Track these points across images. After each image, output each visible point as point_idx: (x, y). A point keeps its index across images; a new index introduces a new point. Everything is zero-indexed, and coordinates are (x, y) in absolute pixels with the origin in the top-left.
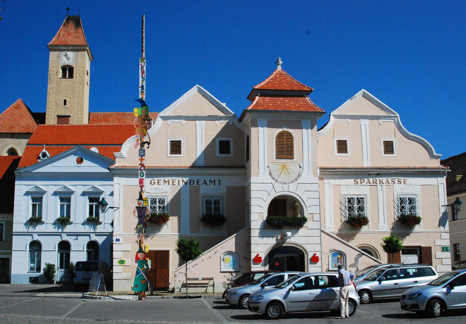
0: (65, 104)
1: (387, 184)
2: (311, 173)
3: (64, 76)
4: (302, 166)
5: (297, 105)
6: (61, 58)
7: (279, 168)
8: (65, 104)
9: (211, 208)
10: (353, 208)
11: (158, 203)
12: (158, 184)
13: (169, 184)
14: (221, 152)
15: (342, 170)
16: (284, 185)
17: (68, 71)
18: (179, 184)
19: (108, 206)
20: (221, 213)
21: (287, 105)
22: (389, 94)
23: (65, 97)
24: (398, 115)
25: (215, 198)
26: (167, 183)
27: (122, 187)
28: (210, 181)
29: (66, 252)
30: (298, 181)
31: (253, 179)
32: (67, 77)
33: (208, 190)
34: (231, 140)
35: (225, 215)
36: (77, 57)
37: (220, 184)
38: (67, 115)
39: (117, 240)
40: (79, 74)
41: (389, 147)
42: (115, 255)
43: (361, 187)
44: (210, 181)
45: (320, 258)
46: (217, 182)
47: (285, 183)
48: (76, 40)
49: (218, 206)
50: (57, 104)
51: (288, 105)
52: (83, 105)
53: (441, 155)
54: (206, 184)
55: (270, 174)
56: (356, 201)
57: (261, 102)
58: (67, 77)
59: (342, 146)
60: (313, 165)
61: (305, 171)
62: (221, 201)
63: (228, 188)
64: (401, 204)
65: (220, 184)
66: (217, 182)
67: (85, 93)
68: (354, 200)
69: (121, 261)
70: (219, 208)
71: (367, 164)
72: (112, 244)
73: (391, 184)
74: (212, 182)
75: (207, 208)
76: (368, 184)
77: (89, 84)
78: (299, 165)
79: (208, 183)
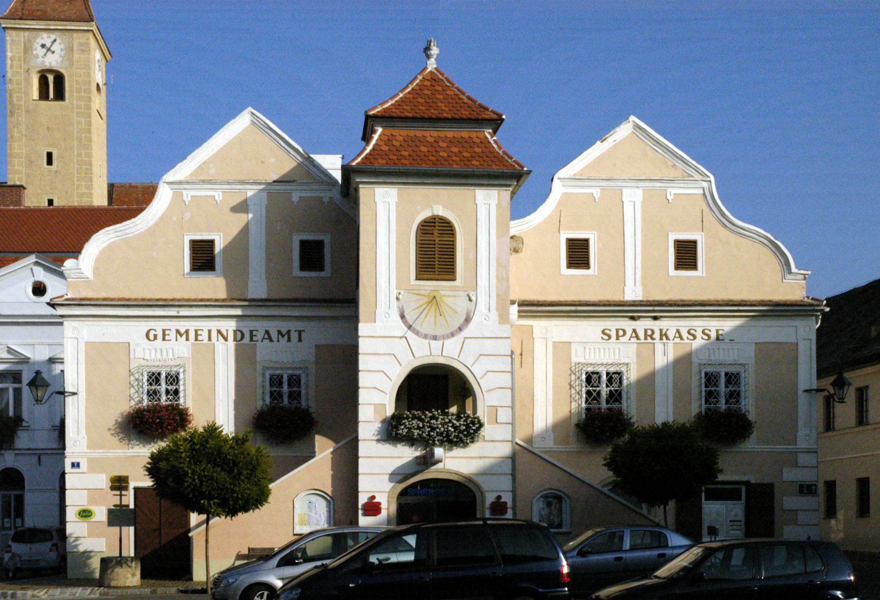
0: (50, 161)
1: (678, 340)
2: (494, 315)
3: (44, 95)
4: (473, 298)
5: (465, 154)
6: (35, 52)
7: (421, 302)
8: (50, 161)
9: (280, 395)
10: (718, 393)
11: (163, 383)
12: (164, 339)
13: (187, 339)
14: (303, 268)
15: (573, 308)
16: (433, 342)
17: (53, 86)
18: (210, 339)
19: (50, 390)
20: (304, 403)
21: (442, 154)
22: (688, 130)
23: (50, 145)
24: (712, 178)
25: (290, 372)
26: (184, 336)
27: (82, 346)
28: (279, 332)
29: (17, 493)
30: (466, 333)
31: (364, 328)
32: (51, 95)
33: (266, 352)
34: (327, 239)
35: (751, 417)
36: (70, 49)
37: (300, 340)
38: (18, 183)
39: (73, 465)
40: (79, 91)
41: (686, 255)
42: (71, 498)
43: (617, 346)
44: (279, 332)
45: (510, 504)
46: (294, 336)
47: (435, 338)
48: (66, 8)
49: (295, 389)
50: (32, 162)
51: (445, 155)
52: (91, 164)
53: (809, 272)
54: (271, 340)
55: (402, 317)
56: (723, 380)
57: (385, 148)
58: (51, 95)
59: (578, 254)
60: (498, 296)
61: (482, 307)
62: (303, 381)
63: (318, 347)
64: (706, 386)
65: (300, 340)
66: (294, 336)
67: (94, 137)
68: (600, 377)
69: (84, 511)
70: (299, 393)
71: (633, 293)
72: (63, 475)
73: (686, 341)
74: (283, 336)
75: (272, 393)
76: (634, 340)
77: (104, 117)
78: (468, 295)
79: (274, 335)
